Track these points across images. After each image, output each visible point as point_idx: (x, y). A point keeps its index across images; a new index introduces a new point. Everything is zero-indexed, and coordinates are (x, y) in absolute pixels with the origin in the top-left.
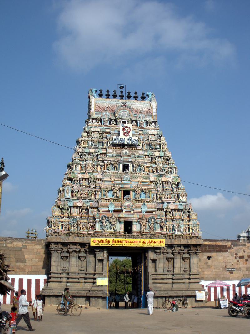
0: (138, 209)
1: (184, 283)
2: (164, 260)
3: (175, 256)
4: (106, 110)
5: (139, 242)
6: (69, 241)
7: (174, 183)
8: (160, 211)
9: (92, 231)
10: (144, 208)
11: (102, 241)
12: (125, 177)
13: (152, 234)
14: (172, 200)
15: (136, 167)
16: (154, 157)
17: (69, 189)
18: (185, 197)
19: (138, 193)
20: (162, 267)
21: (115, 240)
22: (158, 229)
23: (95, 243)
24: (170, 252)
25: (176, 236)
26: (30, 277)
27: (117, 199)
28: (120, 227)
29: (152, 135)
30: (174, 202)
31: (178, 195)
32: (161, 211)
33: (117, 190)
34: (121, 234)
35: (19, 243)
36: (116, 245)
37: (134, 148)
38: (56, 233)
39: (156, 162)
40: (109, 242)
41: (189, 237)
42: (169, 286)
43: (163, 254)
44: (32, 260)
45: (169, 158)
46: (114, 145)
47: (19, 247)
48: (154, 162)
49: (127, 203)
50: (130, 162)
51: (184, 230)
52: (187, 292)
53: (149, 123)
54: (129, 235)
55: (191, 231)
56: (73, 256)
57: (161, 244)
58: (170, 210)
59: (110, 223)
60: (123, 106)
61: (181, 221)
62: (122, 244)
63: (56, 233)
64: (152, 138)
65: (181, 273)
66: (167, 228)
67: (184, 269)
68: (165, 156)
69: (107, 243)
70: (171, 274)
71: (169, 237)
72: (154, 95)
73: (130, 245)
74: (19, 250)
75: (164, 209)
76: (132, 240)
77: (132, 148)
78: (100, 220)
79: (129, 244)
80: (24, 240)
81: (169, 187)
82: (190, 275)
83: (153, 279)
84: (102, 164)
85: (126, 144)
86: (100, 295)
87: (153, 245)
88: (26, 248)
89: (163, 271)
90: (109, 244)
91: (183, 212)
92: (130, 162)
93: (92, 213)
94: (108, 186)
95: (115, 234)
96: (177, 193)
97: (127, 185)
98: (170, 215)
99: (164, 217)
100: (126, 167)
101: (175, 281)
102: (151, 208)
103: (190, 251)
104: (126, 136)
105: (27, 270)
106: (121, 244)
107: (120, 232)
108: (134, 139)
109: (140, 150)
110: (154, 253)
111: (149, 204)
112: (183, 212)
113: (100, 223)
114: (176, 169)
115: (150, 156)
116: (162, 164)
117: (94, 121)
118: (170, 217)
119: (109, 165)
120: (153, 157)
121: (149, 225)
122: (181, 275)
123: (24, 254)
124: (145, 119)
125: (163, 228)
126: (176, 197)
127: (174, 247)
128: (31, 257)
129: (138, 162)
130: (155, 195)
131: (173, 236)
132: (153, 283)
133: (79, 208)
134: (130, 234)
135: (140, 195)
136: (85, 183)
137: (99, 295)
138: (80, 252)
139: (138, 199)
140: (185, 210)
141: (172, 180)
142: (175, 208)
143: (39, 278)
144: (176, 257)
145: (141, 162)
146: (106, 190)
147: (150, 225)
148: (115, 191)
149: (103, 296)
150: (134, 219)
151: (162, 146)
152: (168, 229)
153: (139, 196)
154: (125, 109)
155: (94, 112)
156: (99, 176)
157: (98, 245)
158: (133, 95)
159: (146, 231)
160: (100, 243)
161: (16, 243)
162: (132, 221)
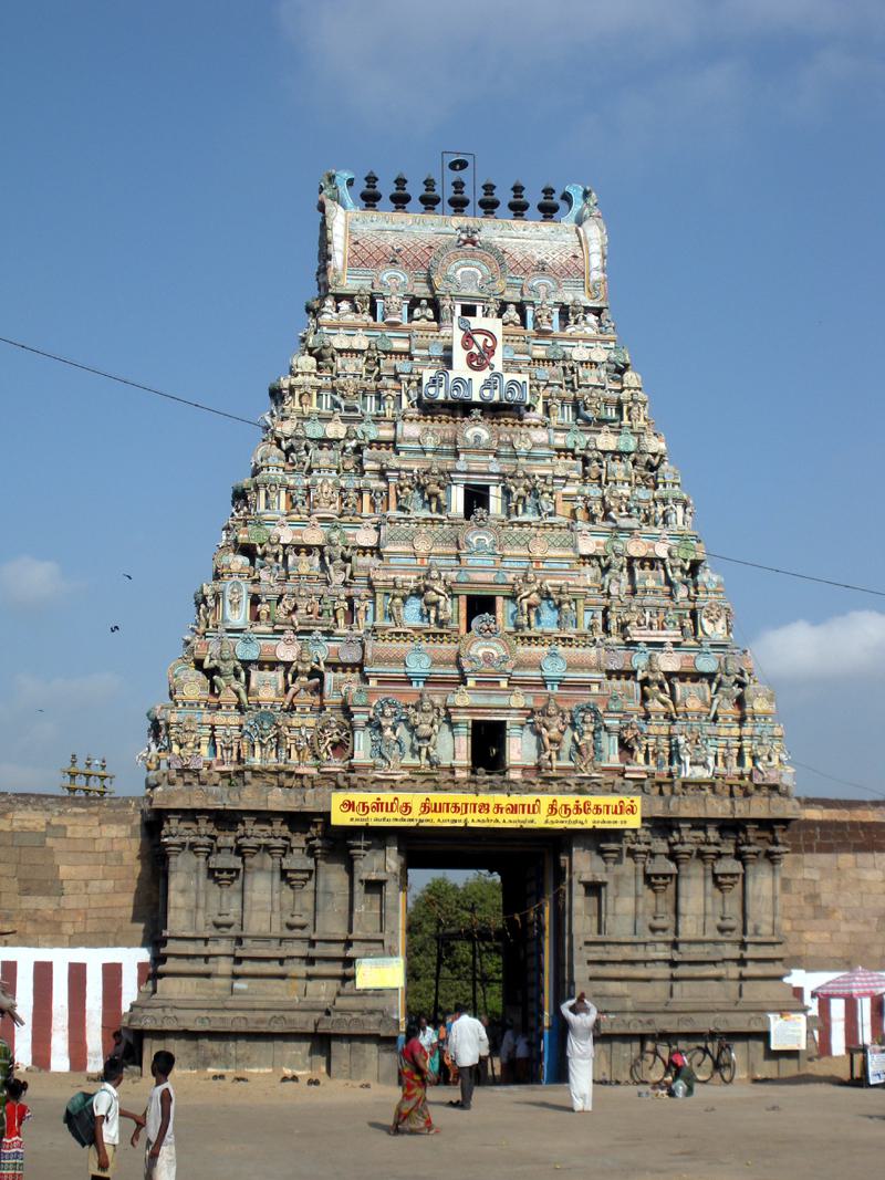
1: (718, 979)
2: (636, 885)
3: (682, 866)
4: (395, 262)
5: (532, 809)
6: (242, 807)
9: (336, 765)
10: (554, 669)
11: (378, 806)
12: (474, 541)
13: (586, 775)
15: (519, 497)
18: (722, 622)
19: (530, 606)
22: (613, 758)
23: (351, 814)
25: (685, 784)
26: (79, 955)
27: (442, 631)
28: (455, 749)
30: (676, 645)
31: (694, 615)
33: (439, 594)
34: (458, 775)
35: (32, 817)
37: (510, 420)
38: (186, 775)
39: (603, 478)
40: (407, 808)
41: (741, 787)
42: (660, 990)
44: (87, 886)
45: (655, 461)
46: (428, 408)
47: (33, 832)
51: (720, 759)
54: (491, 781)
55: (748, 761)
56: (261, 869)
57: (624, 817)
58: (660, 676)
59: (413, 729)
60: (465, 242)
61: (707, 720)
63: (189, 771)
64: (586, 378)
65: (708, 936)
67: (719, 921)
69: (398, 815)
70: (666, 943)
71: (657, 789)
72: (593, 194)
74: (34, 843)
75: (635, 673)
76: (502, 799)
77: (502, 420)
79: (491, 815)
80: (57, 802)
81: (657, 579)
83: (590, 962)
87: (588, 821)
88: (65, 837)
89: (631, 930)
91: (714, 685)
94: (403, 576)
95: (435, 777)
96: (691, 605)
97: (481, 573)
98: (662, 696)
99: (634, 706)
101: (682, 971)
102: (583, 668)
103: (743, 844)
104: (479, 368)
105: (68, 928)
106: (457, 816)
107: (452, 769)
109: (536, 426)
110: (594, 853)
111: (573, 650)
112: (714, 685)
113: (369, 729)
114: (685, 506)
115: (577, 451)
117: (344, 305)
118: (661, 707)
119: (407, 490)
120: (589, 455)
123: (57, 862)
125: (631, 751)
126: (688, 623)
127: (679, 830)
128: (84, 871)
131: (672, 784)
132: (592, 979)
133: (281, 669)
134: (493, 777)
135: (538, 614)
136: (307, 565)
137: (366, 1027)
138: (287, 850)
139: (528, 632)
140: (724, 678)
141: (669, 553)
142: (684, 670)
144: (687, 870)
145: (541, 477)
146: (396, 592)
147: (577, 738)
148: (432, 596)
151: (629, 409)
153: (533, 617)
156: (366, 537)
157: (364, 824)
158: (504, 196)
159: (561, 764)
162: (505, 722)
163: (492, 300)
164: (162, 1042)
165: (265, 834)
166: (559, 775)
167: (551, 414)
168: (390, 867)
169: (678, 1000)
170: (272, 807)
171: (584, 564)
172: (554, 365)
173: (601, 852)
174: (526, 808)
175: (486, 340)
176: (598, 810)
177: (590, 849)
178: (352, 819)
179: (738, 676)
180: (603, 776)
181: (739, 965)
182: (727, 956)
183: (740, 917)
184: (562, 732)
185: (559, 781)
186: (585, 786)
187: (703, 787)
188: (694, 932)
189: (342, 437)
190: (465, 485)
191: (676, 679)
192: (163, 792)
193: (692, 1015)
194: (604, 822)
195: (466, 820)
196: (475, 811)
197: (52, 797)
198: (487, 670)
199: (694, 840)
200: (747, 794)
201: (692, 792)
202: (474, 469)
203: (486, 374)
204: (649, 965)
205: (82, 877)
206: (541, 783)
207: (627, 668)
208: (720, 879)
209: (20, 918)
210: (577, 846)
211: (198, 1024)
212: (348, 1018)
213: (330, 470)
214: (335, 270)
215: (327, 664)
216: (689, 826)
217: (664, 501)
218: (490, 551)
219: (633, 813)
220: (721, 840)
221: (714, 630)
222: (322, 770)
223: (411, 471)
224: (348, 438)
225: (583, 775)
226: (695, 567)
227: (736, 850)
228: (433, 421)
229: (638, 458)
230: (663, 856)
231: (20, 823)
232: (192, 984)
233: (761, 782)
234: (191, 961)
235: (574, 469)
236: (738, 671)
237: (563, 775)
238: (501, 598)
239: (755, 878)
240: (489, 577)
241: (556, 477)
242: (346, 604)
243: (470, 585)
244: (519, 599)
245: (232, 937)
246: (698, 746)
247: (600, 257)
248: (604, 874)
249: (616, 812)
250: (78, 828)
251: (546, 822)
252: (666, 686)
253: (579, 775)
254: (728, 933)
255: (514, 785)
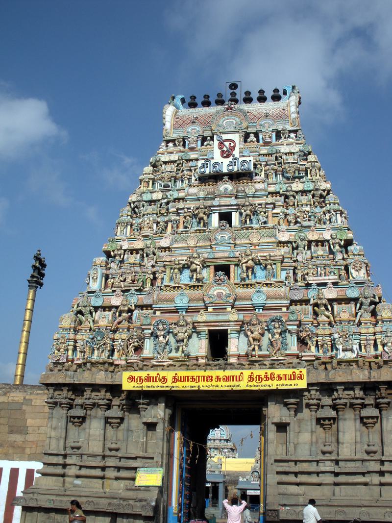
0: (243, 303)
1: (366, 484)
2: (311, 425)
3: (340, 413)
4: (194, 122)
5: (239, 379)
6: (83, 382)
7: (337, 241)
8: (301, 305)
9: (134, 358)
10: (259, 300)
11: (148, 379)
12: (219, 238)
13: (275, 358)
14: (333, 278)
15: (247, 215)
16: (292, 193)
17: (97, 272)
18: (363, 271)
19: (248, 268)
20: (305, 443)
21: (179, 375)
23: (133, 384)
24: (326, 404)
25: (340, 363)
26: (15, 464)
28: (200, 347)
29: (289, 153)
31: (347, 268)
32: (304, 306)
33: (197, 265)
34: (200, 361)
35: (18, 395)
36: (181, 386)
38: (58, 366)
39: (296, 204)
40: (165, 379)
41: (376, 363)
42: (326, 491)
43: (308, 410)
44: (39, 429)
46: (204, 179)
47: (17, 403)
48: (291, 204)
49: (217, 289)
50: (235, 207)
51: (363, 347)
52: (372, 511)
53: (283, 134)
55: (380, 347)
56: (95, 417)
58: (324, 301)
59: (175, 335)
61: (353, 325)
62: (197, 384)
63: (60, 364)
64: (287, 160)
65: (358, 457)
66: (319, 343)
67: (366, 447)
68: (317, 190)
69: (160, 384)
70: (332, 461)
71: (323, 366)
73: (217, 386)
74: (17, 409)
75: (309, 301)
76: (221, 373)
77: (241, 181)
78: (152, 333)
79: (214, 383)
80: (31, 388)
82: (382, 462)
83: (278, 473)
84: (173, 217)
85: (226, 171)
86: (137, 511)
87: (274, 385)
89: (308, 453)
90: (166, 385)
91: (358, 305)
92: (235, 207)
93: (139, 317)
94: (180, 258)
96: (345, 263)
97: (222, 253)
98: (327, 313)
99: (310, 318)
100: (226, 217)
101: (342, 479)
102: (276, 299)
103: (379, 398)
104: (228, 156)
105: (28, 451)
106: (193, 384)
107: (197, 358)
108: (244, 161)
110: (282, 405)
111: (273, 289)
112: (358, 305)
113: (152, 338)
114: (341, 213)
116: (309, 206)
117: (171, 145)
119: (188, 217)
120: (288, 194)
121: (269, 339)
122: (359, 464)
124: (275, 127)
125: (306, 344)
126: (343, 273)
127: (337, 390)
128: (38, 422)
129: (251, 205)
130: (291, 271)
132: (279, 483)
133: (114, 310)
134: (219, 362)
135: (253, 272)
137: (134, 510)
138: (109, 407)
139: (247, 282)
140: (364, 300)
141: (331, 236)
142: (339, 297)
143: (18, 467)
144: (343, 415)
145: (259, 204)
146: (175, 266)
147: (271, 338)
148: (194, 266)
149: (144, 514)
150: (232, 323)
151: (311, 171)
152: (322, 346)
153: (250, 274)
154: (232, 115)
155: (171, 130)
156: (164, 243)
157: (140, 389)
158: (255, 95)
159: (260, 353)
160: (145, 384)
161: (13, 395)
162: (227, 329)
163: (240, 132)
164: (48, 514)
165: (98, 397)
166: (258, 359)
167: (269, 177)
168: (160, 415)
169: (338, 498)
170: (98, 382)
171: (284, 247)
172: (272, 156)
173: (286, 405)
174: (235, 377)
175: (230, 144)
176: (279, 378)
177: (279, 403)
178: (134, 387)
179: (372, 298)
180: (286, 358)
181: (380, 476)
182: (371, 469)
183: (380, 445)
184: (262, 335)
185: (260, 363)
186: (276, 365)
187: (351, 364)
188: (349, 454)
189: (160, 198)
190: (219, 213)
191: (335, 303)
192: (45, 374)
193: (345, 509)
194: (283, 385)
195: (199, 386)
196: (204, 381)
197: (30, 386)
198: (219, 302)
199: (347, 397)
200: (379, 367)
201: (344, 367)
202: (223, 204)
203: (231, 159)
204: (320, 475)
205: (37, 425)
206: (249, 364)
207: (304, 298)
208: (365, 420)
209: (7, 446)
210: (271, 401)
211: (48, 503)
212: (125, 503)
213: (153, 214)
214: (166, 130)
215: (136, 306)
216: (343, 387)
217: (329, 212)
218: (228, 242)
219: (301, 379)
220: (364, 396)
221: (359, 275)
222: (128, 361)
223: (190, 208)
224: (163, 198)
225: (273, 358)
226: (349, 243)
227: (375, 402)
228: (205, 186)
229: (315, 193)
230: (329, 407)
231: (12, 398)
232: (52, 481)
233: (387, 359)
234: (55, 467)
235: (280, 201)
236: (372, 296)
237: (261, 359)
238: (233, 266)
239: (388, 419)
240: (226, 255)
241: (267, 204)
242: (152, 276)
243: (215, 260)
244: (241, 264)
245: (78, 454)
246: (347, 339)
247: (295, 107)
248: (288, 418)
249: (291, 379)
250: (38, 401)
251: (247, 386)
252: (329, 307)
253: (271, 359)
254: (372, 454)
255: (232, 366)
